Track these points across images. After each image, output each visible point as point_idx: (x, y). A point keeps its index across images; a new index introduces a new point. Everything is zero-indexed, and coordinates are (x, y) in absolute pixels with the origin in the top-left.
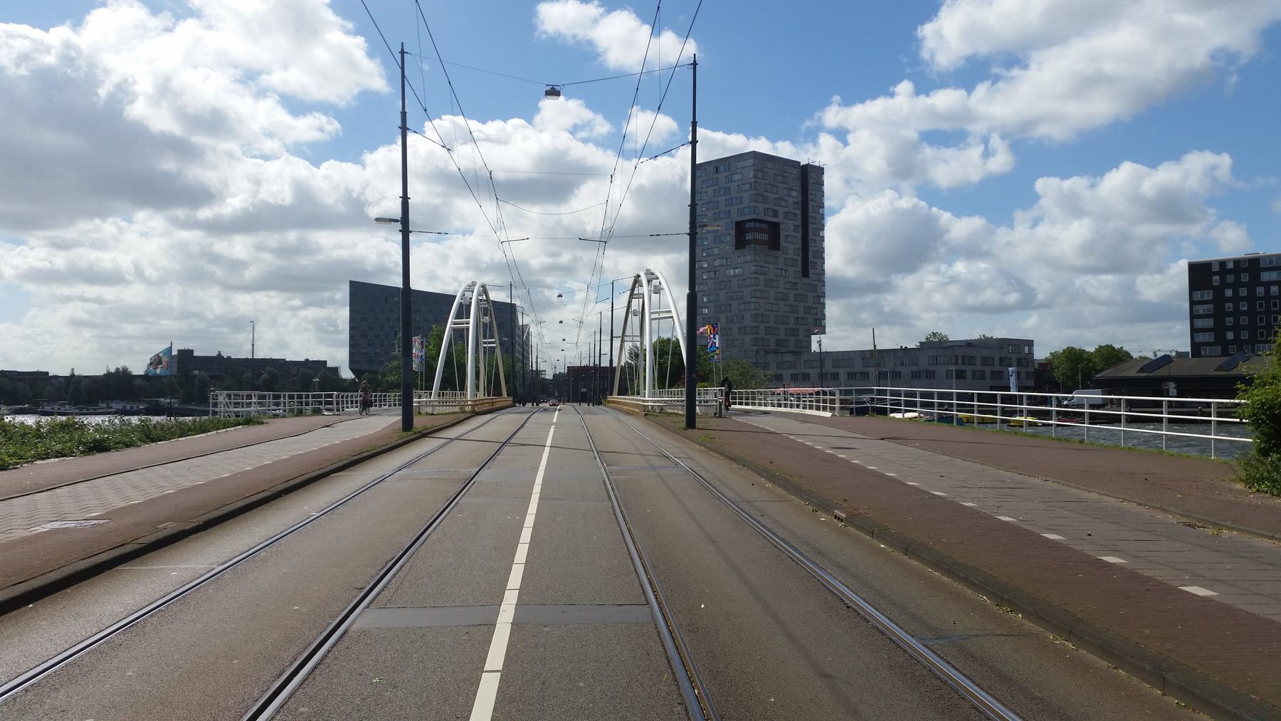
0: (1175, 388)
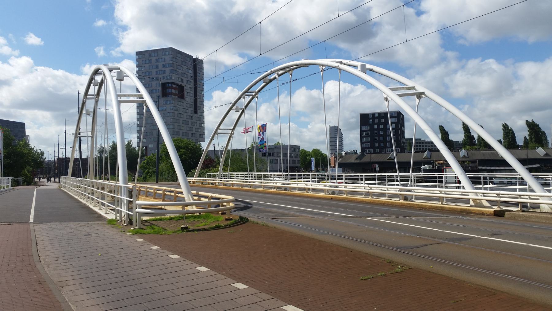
0: (378, 167)
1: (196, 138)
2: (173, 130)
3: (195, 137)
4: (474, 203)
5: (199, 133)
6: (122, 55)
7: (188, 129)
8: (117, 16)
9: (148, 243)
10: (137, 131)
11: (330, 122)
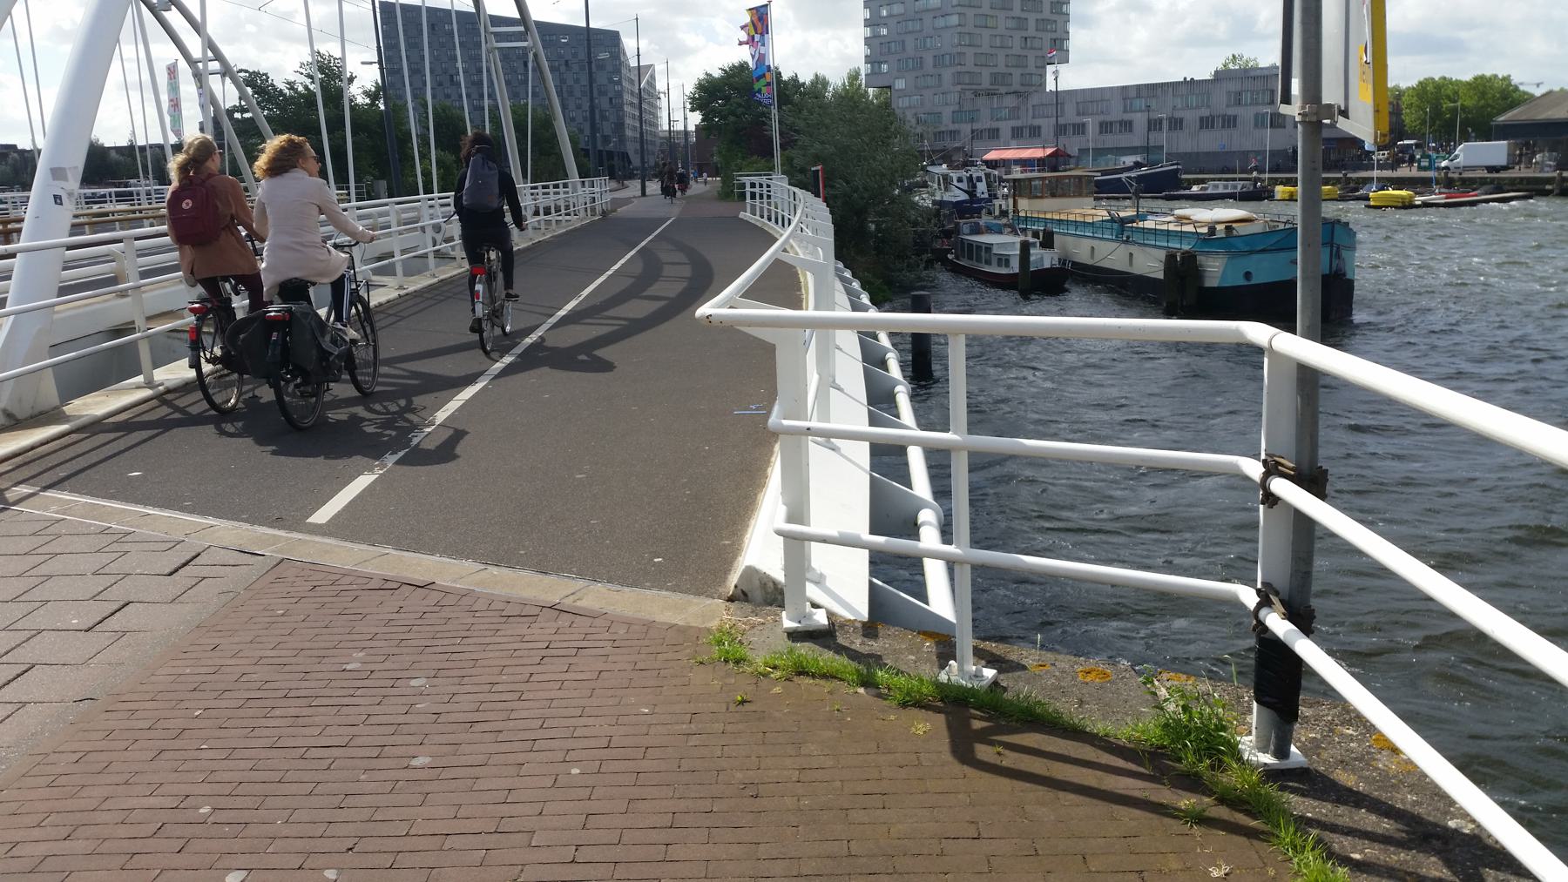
1: (1039, 53)
2: (959, 29)
3: (1032, 48)
4: (310, 523)
5: (1048, 36)
6: (474, 11)
7: (1011, 24)
8: (1098, 302)
9: (14, 11)
10: (866, 39)
11: (1423, 44)
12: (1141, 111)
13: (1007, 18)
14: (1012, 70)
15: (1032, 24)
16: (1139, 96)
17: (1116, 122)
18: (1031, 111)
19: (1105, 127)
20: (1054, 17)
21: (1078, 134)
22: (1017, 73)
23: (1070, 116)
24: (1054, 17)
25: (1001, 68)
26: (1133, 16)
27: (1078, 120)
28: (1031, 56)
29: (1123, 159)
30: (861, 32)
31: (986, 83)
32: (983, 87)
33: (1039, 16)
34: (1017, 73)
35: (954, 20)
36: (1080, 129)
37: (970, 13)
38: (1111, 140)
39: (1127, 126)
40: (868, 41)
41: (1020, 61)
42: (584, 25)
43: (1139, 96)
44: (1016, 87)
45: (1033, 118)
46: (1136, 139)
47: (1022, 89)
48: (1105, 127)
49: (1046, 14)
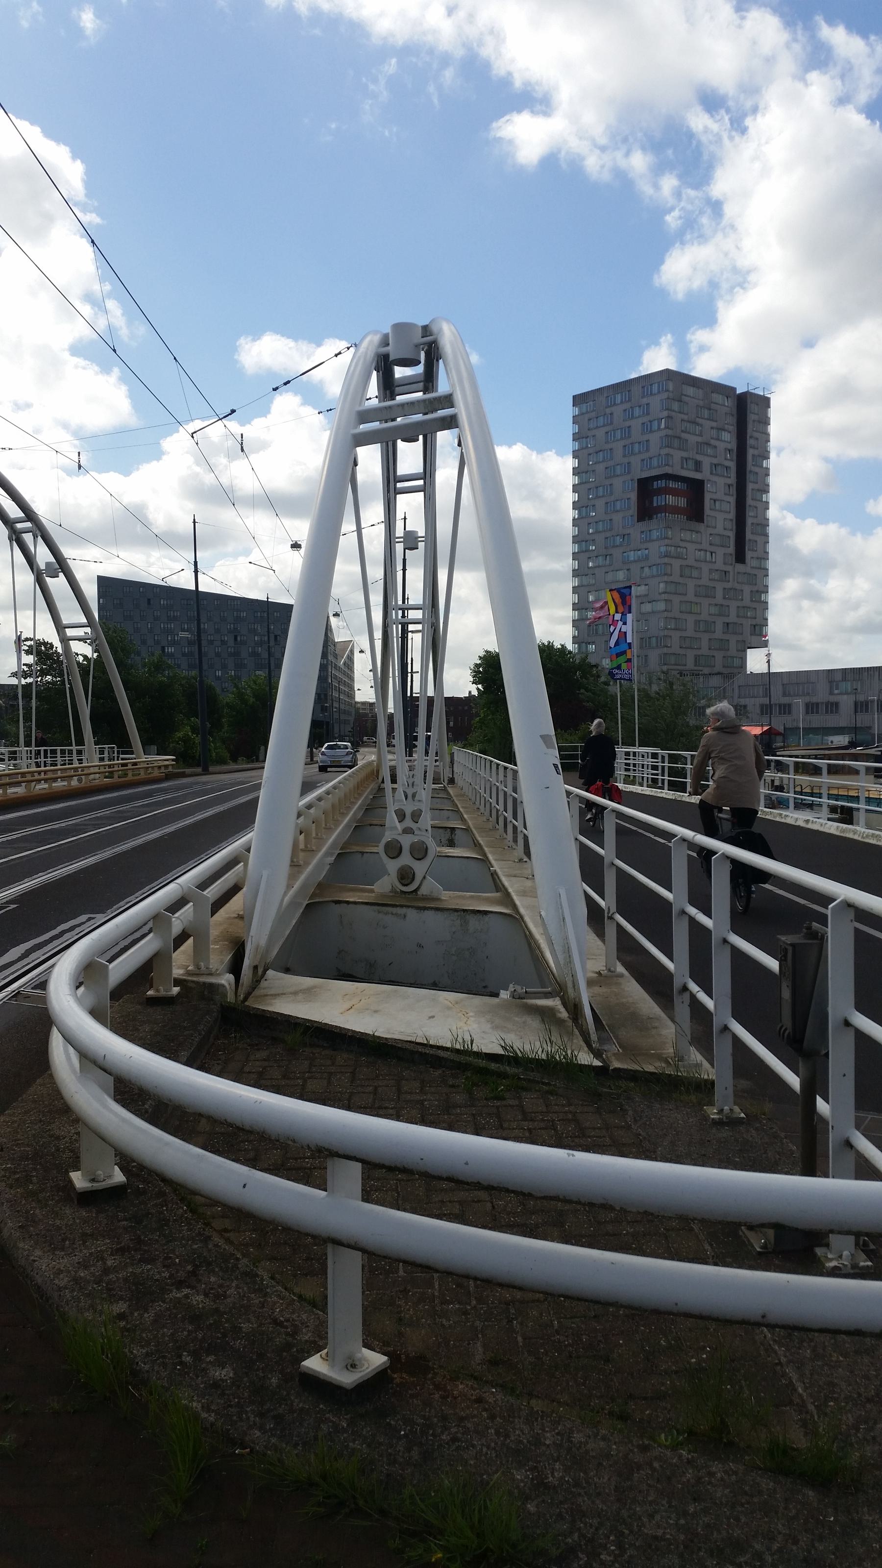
1: (740, 638)
5: (747, 624)
7: (713, 610)
12: (847, 693)
13: (710, 605)
14: (715, 653)
15: (733, 612)
16: (844, 679)
17: (822, 703)
18: (736, 691)
19: (811, 708)
20: (754, 605)
21: (832, 712)
22: (719, 655)
23: (777, 697)
24: (754, 605)
25: (705, 651)
26: (806, 604)
27: (785, 700)
28: (733, 639)
29: (831, 738)
30: (568, 613)
31: (690, 664)
32: (687, 668)
33: (740, 604)
34: (719, 655)
35: (661, 606)
36: (786, 709)
37: (676, 599)
38: (817, 720)
39: (833, 707)
40: (575, 623)
41: (723, 645)
42: (194, 588)
43: (844, 679)
44: (718, 668)
45: (739, 697)
46: (843, 719)
47: (725, 671)
48: (811, 708)
49: (747, 602)
